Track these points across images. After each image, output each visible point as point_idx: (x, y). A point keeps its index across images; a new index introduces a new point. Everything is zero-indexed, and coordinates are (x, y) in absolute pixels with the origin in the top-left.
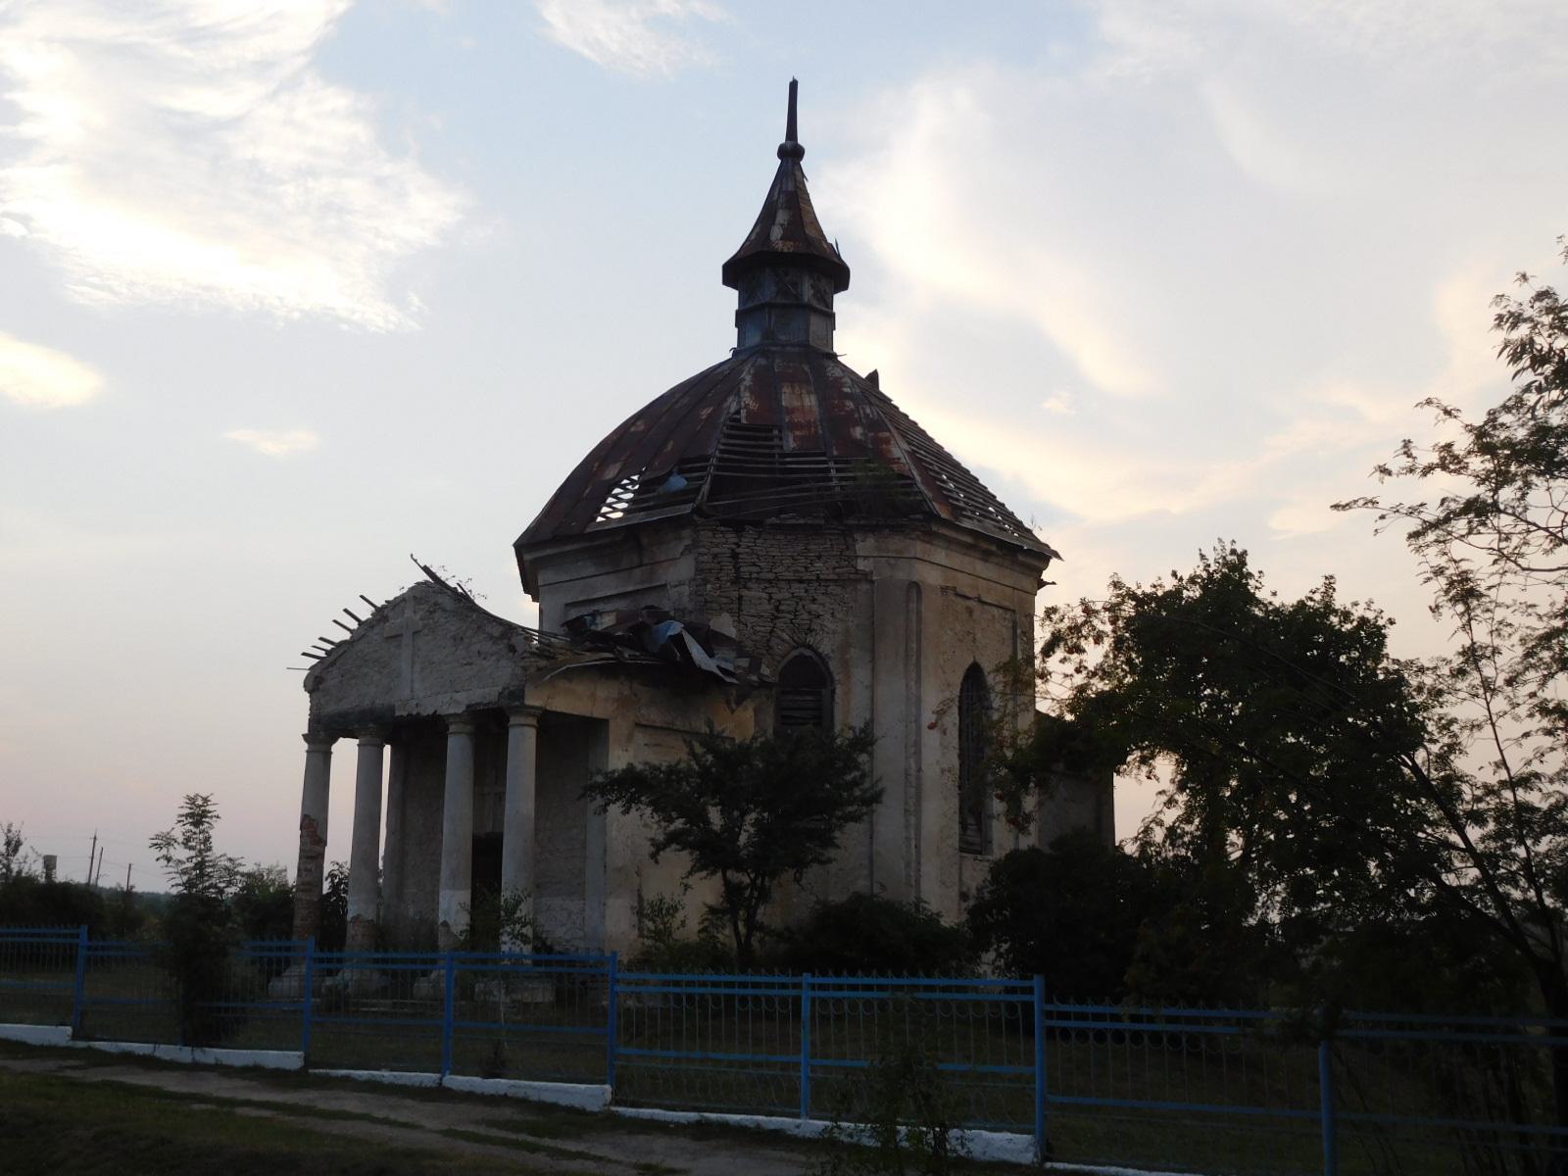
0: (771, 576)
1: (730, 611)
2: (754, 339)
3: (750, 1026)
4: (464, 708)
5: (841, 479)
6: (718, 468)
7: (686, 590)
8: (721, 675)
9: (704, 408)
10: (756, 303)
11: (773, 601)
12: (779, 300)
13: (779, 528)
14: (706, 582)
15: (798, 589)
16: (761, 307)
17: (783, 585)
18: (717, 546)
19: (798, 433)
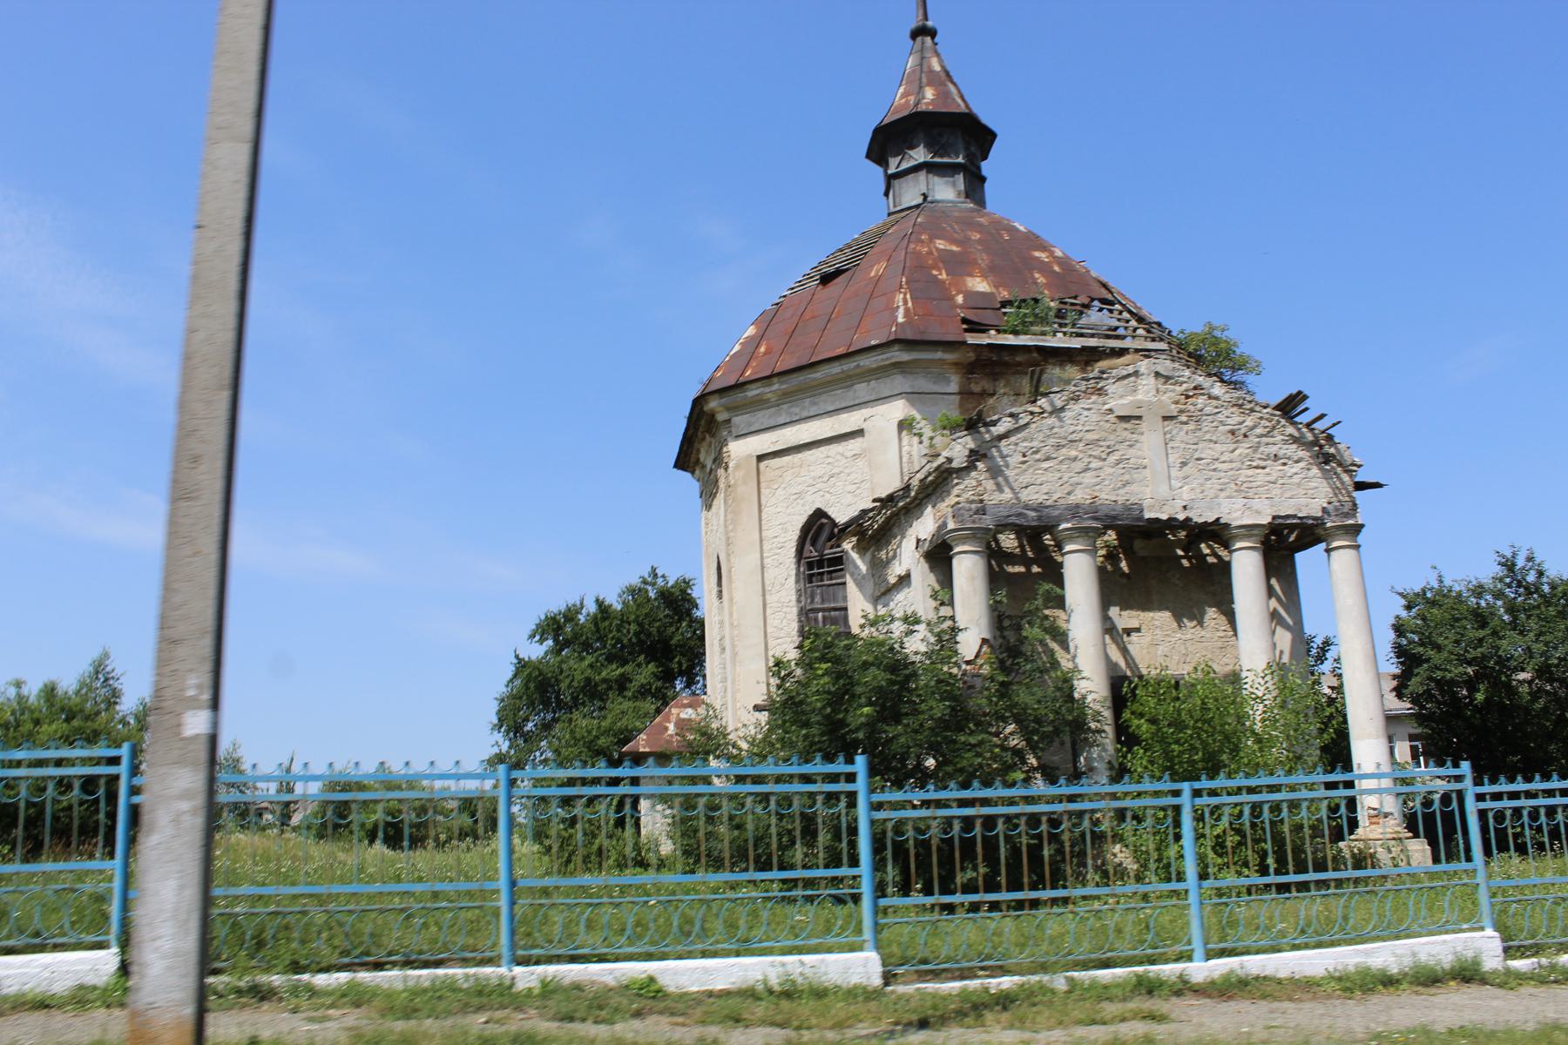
10: (912, 163)
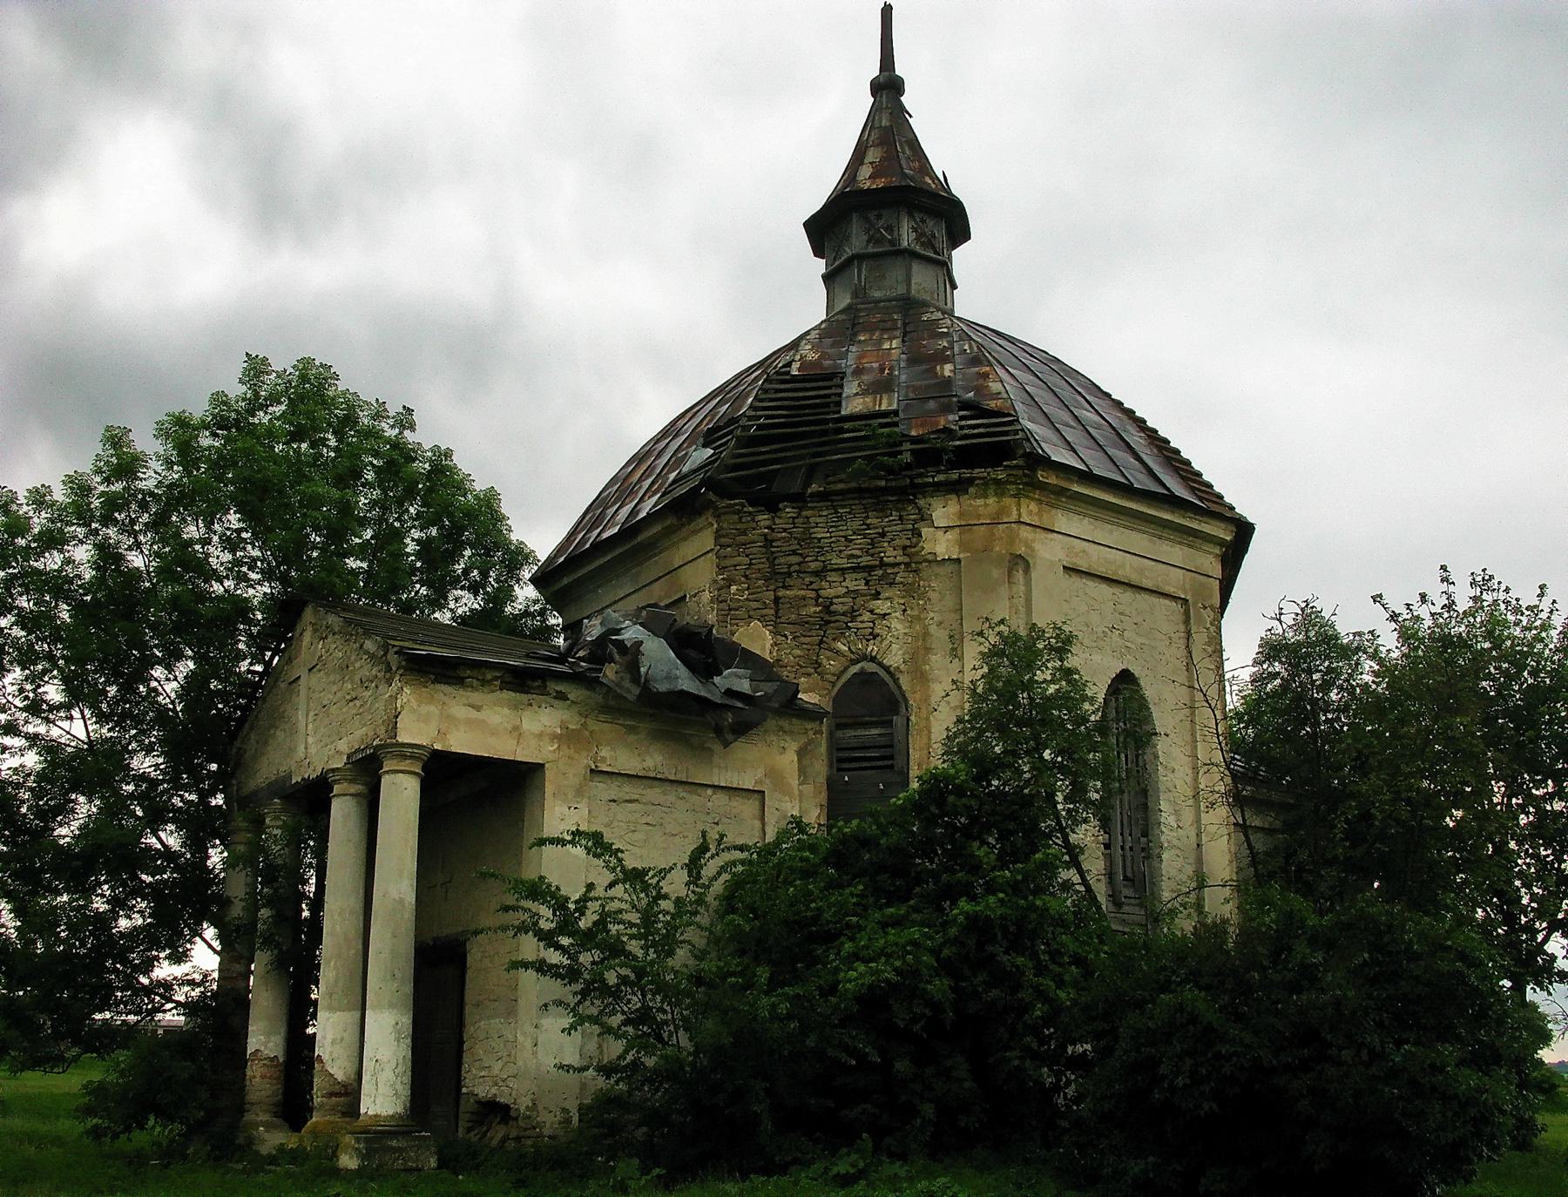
1: (762, 619)
2: (844, 301)
12: (871, 250)
13: (823, 496)
14: (730, 581)
15: (854, 583)
16: (848, 262)
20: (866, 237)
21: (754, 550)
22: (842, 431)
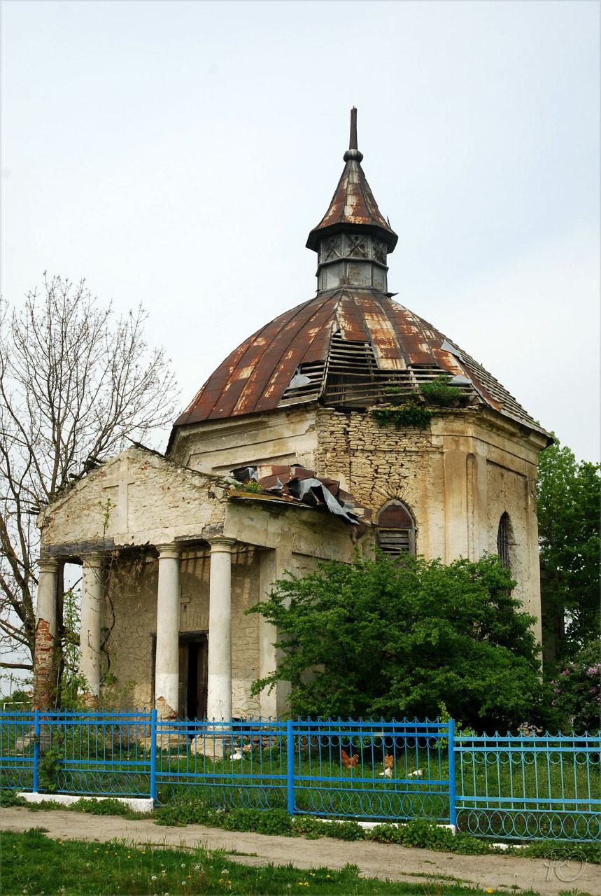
0: (372, 448)
3: (373, 763)
4: (173, 540)
5: (418, 379)
6: (330, 369)
7: (312, 457)
8: (348, 517)
9: (312, 328)
10: (335, 259)
11: (373, 466)
12: (352, 257)
15: (391, 457)
17: (381, 455)
18: (333, 426)
19: (382, 346)
20: (349, 249)
21: (338, 435)
22: (386, 379)
